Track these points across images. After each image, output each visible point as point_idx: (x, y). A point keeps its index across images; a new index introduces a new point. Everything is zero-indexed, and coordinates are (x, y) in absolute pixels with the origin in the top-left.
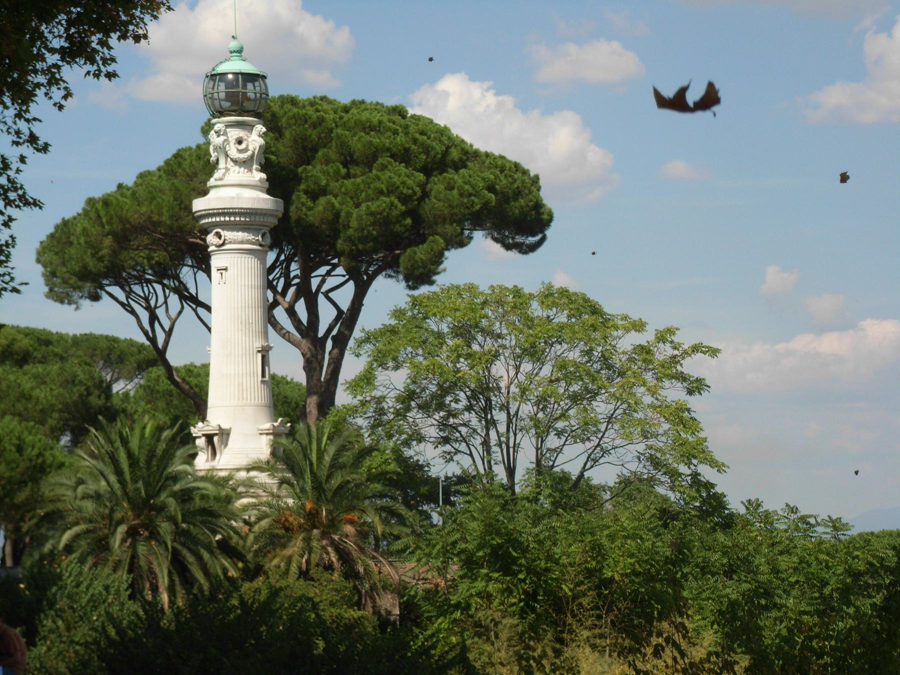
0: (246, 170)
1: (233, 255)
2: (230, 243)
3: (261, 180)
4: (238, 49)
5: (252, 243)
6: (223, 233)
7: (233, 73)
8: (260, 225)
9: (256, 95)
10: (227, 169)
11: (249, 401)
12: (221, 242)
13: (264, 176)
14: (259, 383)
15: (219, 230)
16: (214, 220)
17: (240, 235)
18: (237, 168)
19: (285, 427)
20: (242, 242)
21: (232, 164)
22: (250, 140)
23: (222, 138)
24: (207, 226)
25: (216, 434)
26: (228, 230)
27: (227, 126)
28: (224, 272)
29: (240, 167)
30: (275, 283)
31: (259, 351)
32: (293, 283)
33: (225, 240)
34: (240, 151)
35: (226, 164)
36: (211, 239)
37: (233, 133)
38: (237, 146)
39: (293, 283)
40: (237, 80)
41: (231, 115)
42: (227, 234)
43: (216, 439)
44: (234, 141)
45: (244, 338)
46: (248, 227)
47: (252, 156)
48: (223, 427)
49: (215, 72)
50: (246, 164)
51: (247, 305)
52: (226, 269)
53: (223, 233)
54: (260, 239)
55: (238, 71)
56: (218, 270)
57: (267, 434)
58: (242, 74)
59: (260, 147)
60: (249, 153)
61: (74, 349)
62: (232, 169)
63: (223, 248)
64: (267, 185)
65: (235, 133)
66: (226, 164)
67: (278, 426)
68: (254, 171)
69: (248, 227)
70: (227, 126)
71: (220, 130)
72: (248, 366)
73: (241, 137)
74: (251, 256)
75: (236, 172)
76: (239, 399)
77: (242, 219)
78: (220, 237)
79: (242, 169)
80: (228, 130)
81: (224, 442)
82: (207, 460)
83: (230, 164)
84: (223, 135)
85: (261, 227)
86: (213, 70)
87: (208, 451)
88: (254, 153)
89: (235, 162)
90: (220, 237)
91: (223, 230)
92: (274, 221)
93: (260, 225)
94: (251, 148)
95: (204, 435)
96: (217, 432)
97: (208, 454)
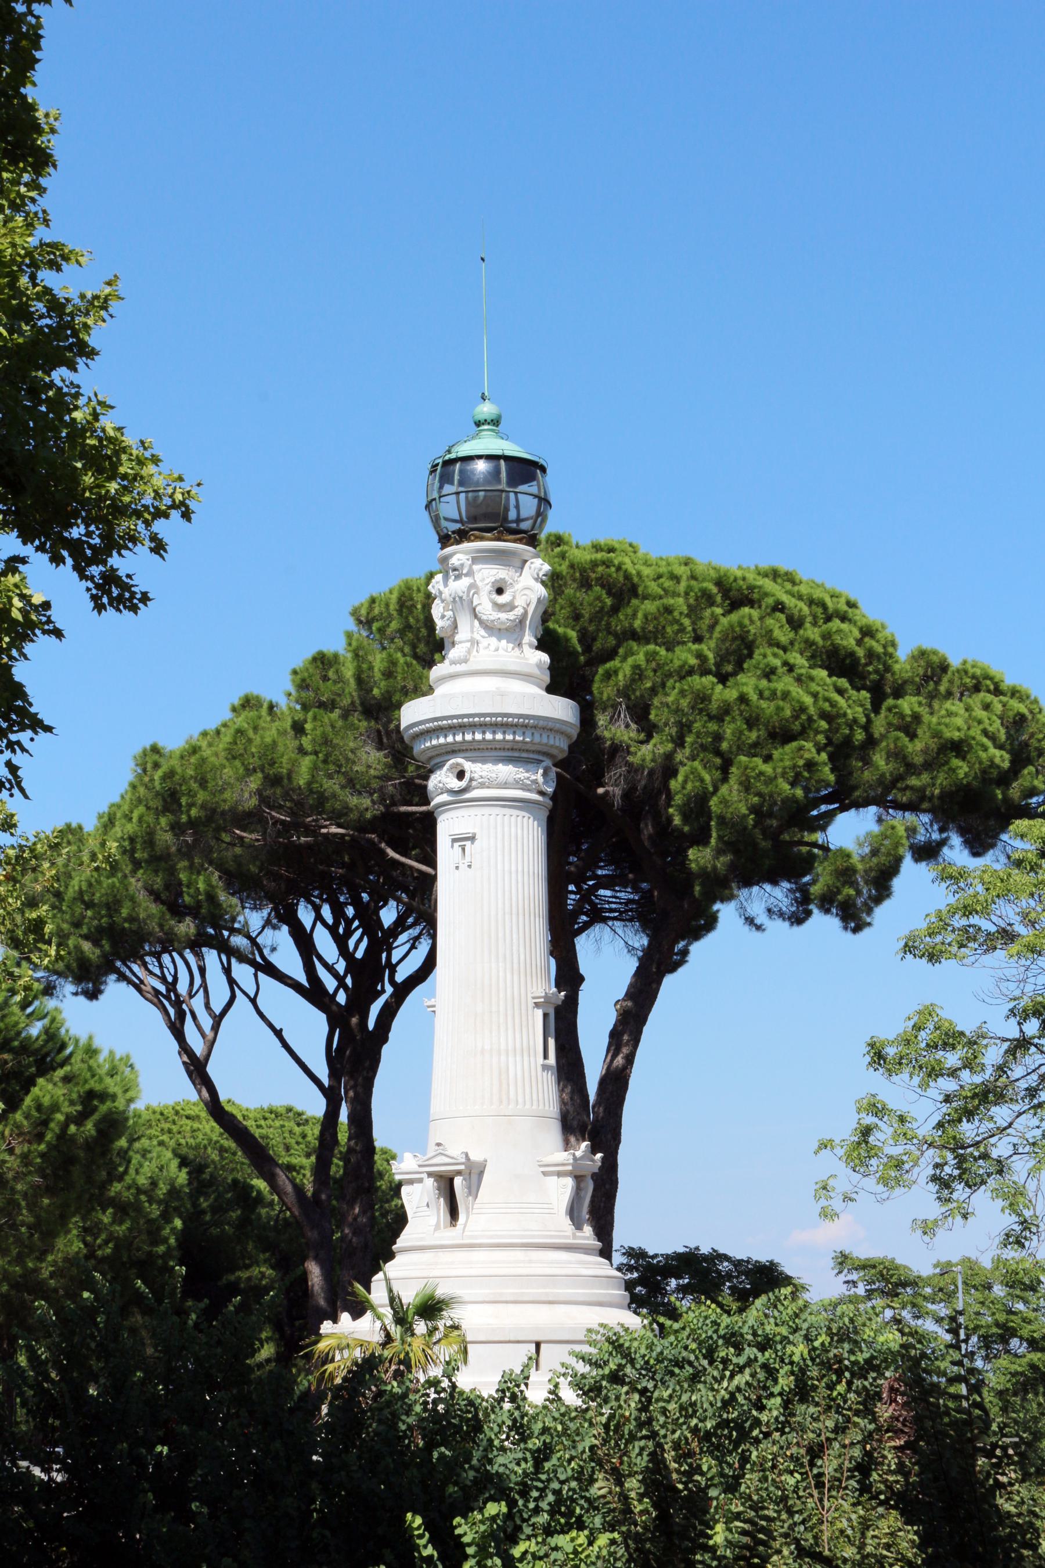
0: (511, 645)
1: (487, 811)
2: (482, 786)
3: (539, 665)
4: (493, 417)
5: (525, 788)
6: (468, 766)
7: (489, 458)
8: (539, 752)
9: (512, 522)
10: (475, 643)
11: (528, 1106)
12: (463, 784)
13: (545, 658)
14: (540, 1069)
15: (460, 760)
16: (459, 738)
17: (505, 771)
18: (493, 640)
19: (593, 1161)
20: (505, 785)
21: (483, 632)
22: (518, 586)
23: (465, 581)
24: (430, 754)
25: (459, 1173)
26: (484, 760)
27: (475, 560)
28: (468, 843)
29: (499, 640)
30: (224, 958)
31: (537, 1005)
32: (361, 930)
33: (471, 780)
34: (500, 607)
35: (472, 632)
36: (441, 780)
37: (485, 572)
38: (495, 596)
39: (361, 930)
40: (497, 472)
41: (482, 539)
42: (474, 769)
43: (458, 1182)
44: (489, 588)
45: (509, 976)
46: (516, 754)
47: (521, 621)
48: (473, 1157)
49: (453, 456)
50: (512, 632)
51: (507, 909)
52: (472, 839)
53: (468, 766)
54: (541, 779)
55: (499, 453)
56: (454, 841)
57: (559, 1174)
58: (507, 458)
59: (539, 600)
60: (519, 611)
61: (970, 1106)
62: (484, 643)
63: (467, 796)
64: (547, 679)
65: (488, 574)
66: (472, 632)
67: (582, 1158)
68: (526, 648)
69: (516, 754)
70: (475, 560)
71: (462, 565)
72: (518, 1036)
73: (503, 580)
74: (527, 815)
75: (492, 648)
76: (501, 1102)
77: (509, 737)
78: (461, 775)
79: (504, 642)
80: (475, 567)
81: (473, 1190)
82: (437, 1227)
83: (480, 633)
84: (466, 575)
85: (541, 758)
86: (449, 452)
87: (439, 1209)
88: (526, 613)
89: (490, 628)
90: (461, 775)
91: (467, 759)
92: (561, 745)
93: (539, 752)
94: (520, 602)
95: (430, 1174)
96: (462, 1167)
97: (439, 1209)
